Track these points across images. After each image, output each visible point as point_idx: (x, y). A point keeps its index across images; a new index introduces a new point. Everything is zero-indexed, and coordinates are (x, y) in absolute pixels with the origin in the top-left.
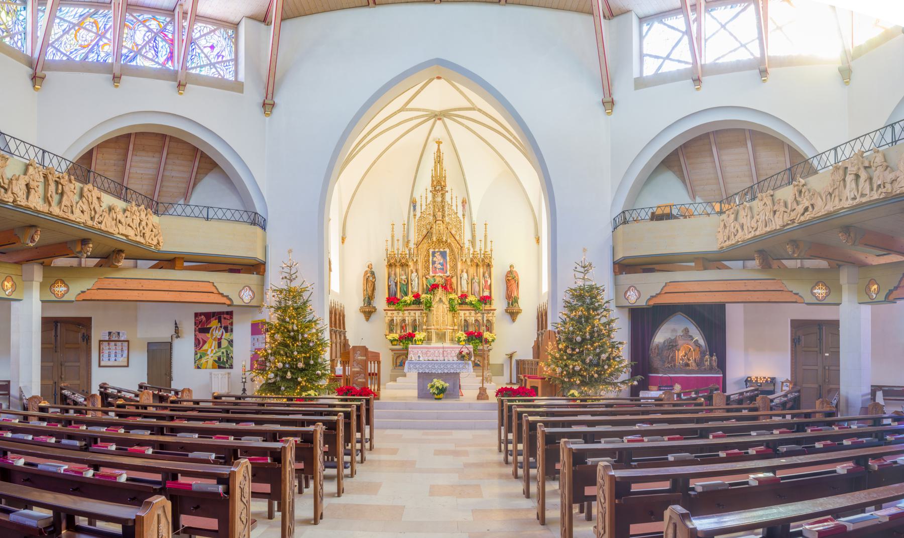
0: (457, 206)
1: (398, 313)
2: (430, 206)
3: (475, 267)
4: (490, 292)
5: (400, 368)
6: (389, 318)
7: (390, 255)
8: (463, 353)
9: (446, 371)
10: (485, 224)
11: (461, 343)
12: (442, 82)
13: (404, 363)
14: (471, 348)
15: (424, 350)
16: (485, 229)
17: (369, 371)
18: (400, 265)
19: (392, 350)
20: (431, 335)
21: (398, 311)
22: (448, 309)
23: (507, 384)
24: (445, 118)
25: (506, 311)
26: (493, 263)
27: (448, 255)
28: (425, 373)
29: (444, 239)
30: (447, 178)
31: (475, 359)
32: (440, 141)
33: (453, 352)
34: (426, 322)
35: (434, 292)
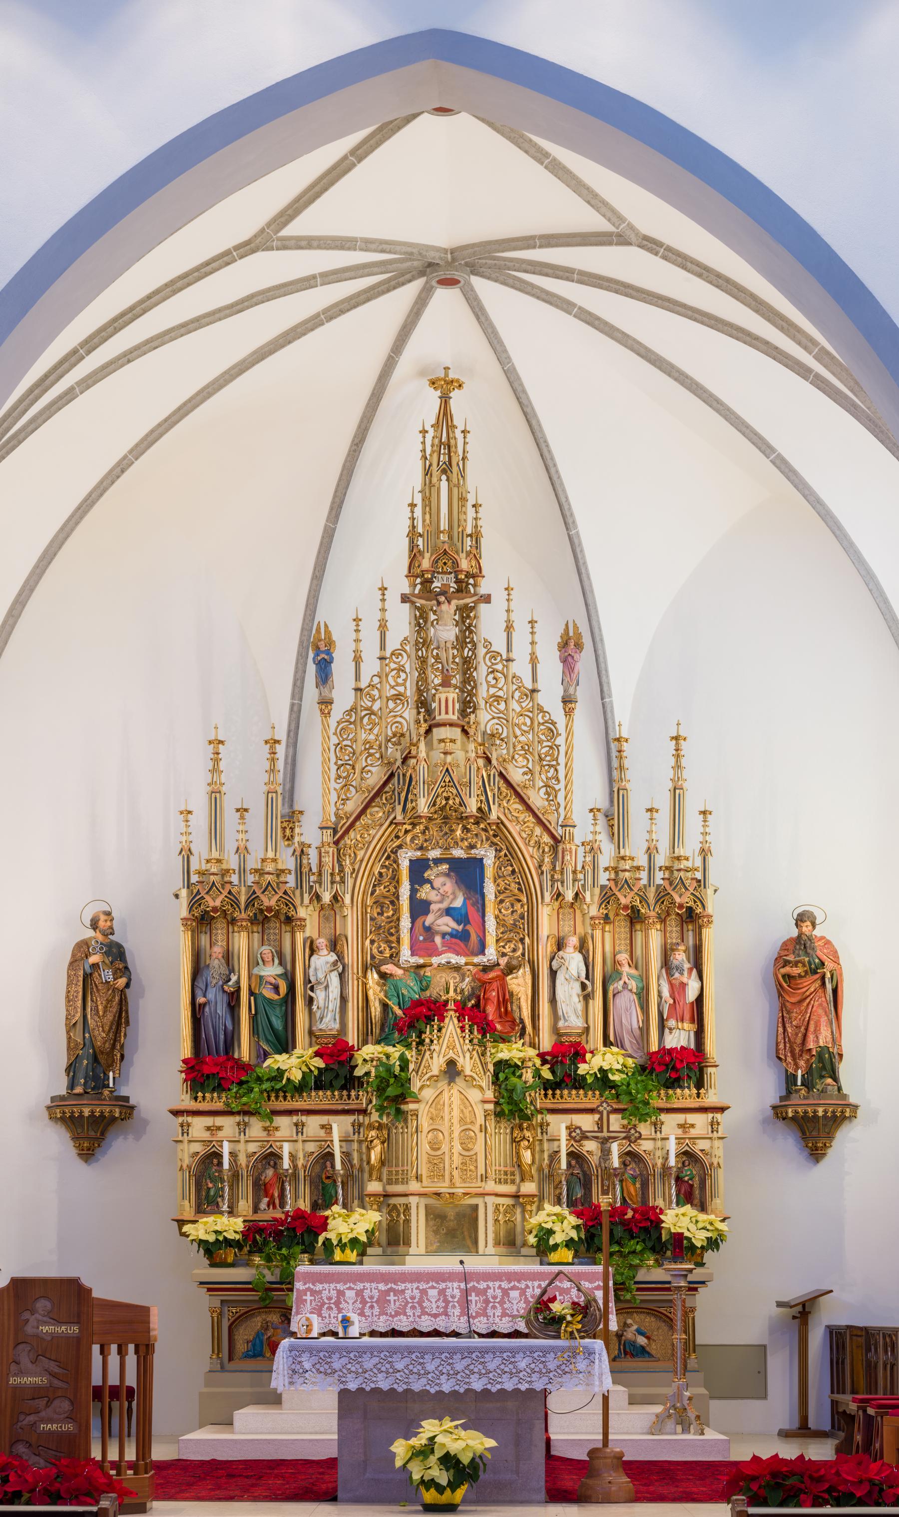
0: (534, 661)
1: (243, 1128)
2: (404, 660)
3: (622, 927)
4: (700, 1034)
5: (251, 1364)
6: (197, 1147)
7: (201, 873)
8: (556, 1307)
9: (478, 1385)
10: (676, 738)
11: (554, 1257)
12: (464, 121)
13: (274, 1347)
14: (590, 1277)
15: (372, 1290)
16: (672, 762)
17: (96, 1379)
18: (253, 921)
19: (212, 1287)
20: (407, 1222)
21: (238, 1118)
22: (491, 1107)
23: (785, 1434)
24: (476, 281)
25: (778, 1112)
26: (713, 905)
27: (489, 873)
28: (376, 1391)
29: (472, 806)
30: (483, 542)
31: (624, 1326)
32: (452, 375)
33: (514, 1294)
34: (382, 1163)
35: (421, 1033)
